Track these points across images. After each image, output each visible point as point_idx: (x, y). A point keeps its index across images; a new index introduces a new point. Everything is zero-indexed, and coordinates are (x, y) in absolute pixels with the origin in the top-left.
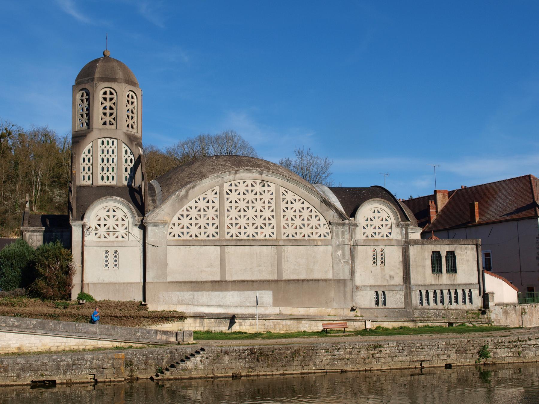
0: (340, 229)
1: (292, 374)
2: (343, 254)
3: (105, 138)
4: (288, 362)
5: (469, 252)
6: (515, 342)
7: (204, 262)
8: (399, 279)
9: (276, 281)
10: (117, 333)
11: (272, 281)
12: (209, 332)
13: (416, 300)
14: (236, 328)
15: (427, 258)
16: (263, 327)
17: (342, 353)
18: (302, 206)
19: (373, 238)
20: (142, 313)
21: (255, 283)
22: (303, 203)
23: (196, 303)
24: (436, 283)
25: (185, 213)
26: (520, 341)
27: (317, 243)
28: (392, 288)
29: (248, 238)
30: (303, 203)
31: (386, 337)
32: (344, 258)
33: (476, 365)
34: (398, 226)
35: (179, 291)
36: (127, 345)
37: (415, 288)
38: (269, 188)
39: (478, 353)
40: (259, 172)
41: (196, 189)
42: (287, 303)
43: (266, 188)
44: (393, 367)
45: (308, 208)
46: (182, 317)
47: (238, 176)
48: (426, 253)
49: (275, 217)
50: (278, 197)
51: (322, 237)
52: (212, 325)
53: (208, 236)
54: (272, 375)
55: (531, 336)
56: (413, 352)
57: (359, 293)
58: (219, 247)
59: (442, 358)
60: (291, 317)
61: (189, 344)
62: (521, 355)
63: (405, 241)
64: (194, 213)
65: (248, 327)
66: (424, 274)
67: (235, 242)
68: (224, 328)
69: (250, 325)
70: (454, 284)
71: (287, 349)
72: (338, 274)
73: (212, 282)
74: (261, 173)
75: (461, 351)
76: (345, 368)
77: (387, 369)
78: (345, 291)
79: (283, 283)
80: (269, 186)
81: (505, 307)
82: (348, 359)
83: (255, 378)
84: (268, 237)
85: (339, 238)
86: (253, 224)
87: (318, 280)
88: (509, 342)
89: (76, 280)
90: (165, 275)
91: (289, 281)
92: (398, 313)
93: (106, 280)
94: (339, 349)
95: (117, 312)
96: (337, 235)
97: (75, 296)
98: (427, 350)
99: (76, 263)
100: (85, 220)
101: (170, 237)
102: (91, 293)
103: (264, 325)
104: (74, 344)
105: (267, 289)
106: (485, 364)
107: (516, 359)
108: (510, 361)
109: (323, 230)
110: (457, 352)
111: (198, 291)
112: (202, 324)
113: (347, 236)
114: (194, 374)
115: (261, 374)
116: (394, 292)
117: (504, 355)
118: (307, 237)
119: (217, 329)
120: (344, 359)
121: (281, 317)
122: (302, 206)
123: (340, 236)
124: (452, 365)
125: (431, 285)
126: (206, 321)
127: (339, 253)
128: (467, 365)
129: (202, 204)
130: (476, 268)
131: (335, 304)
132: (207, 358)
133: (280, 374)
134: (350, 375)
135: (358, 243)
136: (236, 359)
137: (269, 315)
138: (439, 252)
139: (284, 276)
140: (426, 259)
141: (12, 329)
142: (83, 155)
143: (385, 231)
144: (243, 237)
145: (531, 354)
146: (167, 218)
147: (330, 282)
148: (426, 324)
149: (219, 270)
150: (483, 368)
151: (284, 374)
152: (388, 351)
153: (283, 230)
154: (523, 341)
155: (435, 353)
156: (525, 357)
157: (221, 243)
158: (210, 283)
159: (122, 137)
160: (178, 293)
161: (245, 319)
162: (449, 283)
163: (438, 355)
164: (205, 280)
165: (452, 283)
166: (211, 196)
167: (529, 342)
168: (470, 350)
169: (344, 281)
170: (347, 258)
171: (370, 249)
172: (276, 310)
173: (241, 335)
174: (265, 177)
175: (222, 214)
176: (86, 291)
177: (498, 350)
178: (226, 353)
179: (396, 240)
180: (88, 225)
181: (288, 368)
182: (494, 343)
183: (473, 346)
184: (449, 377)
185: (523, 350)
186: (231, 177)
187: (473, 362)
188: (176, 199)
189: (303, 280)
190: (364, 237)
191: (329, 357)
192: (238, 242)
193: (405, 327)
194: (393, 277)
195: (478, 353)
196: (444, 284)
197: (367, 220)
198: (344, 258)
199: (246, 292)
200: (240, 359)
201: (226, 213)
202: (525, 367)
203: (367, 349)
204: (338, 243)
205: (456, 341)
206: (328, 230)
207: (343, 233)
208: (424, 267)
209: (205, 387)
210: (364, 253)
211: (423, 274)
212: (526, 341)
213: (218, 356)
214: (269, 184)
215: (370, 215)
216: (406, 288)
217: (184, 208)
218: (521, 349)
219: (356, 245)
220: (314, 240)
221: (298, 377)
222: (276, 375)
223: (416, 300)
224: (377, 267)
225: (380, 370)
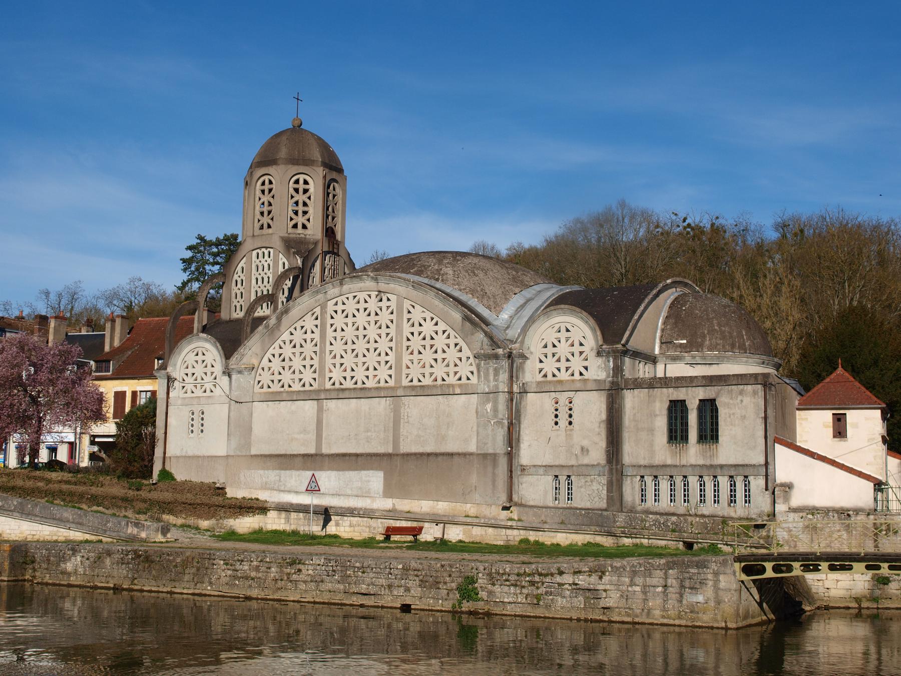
0: (492, 364)
1: (182, 594)
2: (495, 410)
3: (260, 248)
5: (747, 400)
6: (529, 575)
7: (284, 425)
8: (598, 454)
9: (389, 456)
10: (89, 521)
12: (295, 533)
13: (633, 496)
14: (331, 529)
15: (658, 413)
16: (367, 530)
17: (246, 567)
18: (436, 328)
19: (555, 379)
20: (218, 500)
21: (359, 458)
22: (436, 324)
23: (282, 488)
24: (674, 463)
26: (540, 575)
27: (454, 390)
28: (584, 470)
29: (411, 384)
30: (436, 324)
31: (308, 549)
32: (495, 416)
33: (454, 613)
34: (599, 354)
35: (263, 469)
37: (629, 471)
38: (388, 303)
39: (459, 589)
40: (372, 278)
43: (384, 304)
44: (317, 600)
45: (444, 332)
46: (260, 508)
47: (346, 287)
48: (658, 405)
49: (394, 349)
53: (304, 385)
54: (158, 592)
56: (349, 576)
58: (315, 402)
59: (395, 593)
60: (408, 515)
61: (155, 542)
62: (541, 603)
63: (613, 383)
64: (288, 351)
65: (347, 529)
66: (651, 445)
67: (336, 393)
68: (316, 529)
69: (350, 526)
70: (712, 466)
72: (486, 444)
73: (304, 456)
74: (376, 280)
75: (430, 583)
77: (308, 602)
78: (494, 474)
79: (399, 458)
80: (388, 300)
81: (810, 516)
82: (253, 579)
83: (139, 594)
84: (382, 384)
85: (489, 381)
87: (451, 455)
88: (518, 575)
90: (249, 445)
93: (190, 453)
94: (242, 561)
98: (371, 575)
100: (169, 369)
101: (257, 389)
102: (173, 471)
103: (370, 527)
104: (48, 533)
105: (376, 469)
106: (470, 613)
107: (529, 609)
108: (519, 611)
109: (465, 369)
111: (286, 469)
112: (288, 520)
113: (504, 376)
114: (73, 580)
115: (145, 588)
116: (588, 479)
117: (508, 598)
118: (439, 382)
119: (306, 529)
121: (412, 516)
122: (436, 328)
123: (491, 378)
124: (412, 607)
126: (293, 515)
127: (489, 407)
128: (438, 611)
129: (298, 337)
130: (762, 433)
131: (477, 497)
132: (88, 559)
133: (167, 592)
135: (528, 389)
136: (118, 563)
138: (685, 401)
139: (401, 447)
140: (656, 416)
142: (236, 277)
143: (577, 364)
144: (349, 384)
145: (560, 601)
146: (255, 362)
147: (471, 457)
148: (638, 541)
149: (315, 437)
152: (310, 572)
154: (546, 575)
156: (548, 607)
157: (316, 395)
158: (300, 459)
159: (278, 244)
160: (261, 472)
162: (701, 462)
163: (390, 586)
164: (295, 453)
165: (708, 463)
166: (309, 323)
167: (558, 579)
168: (445, 583)
169: (494, 456)
170: (500, 416)
172: (388, 504)
174: (382, 286)
175: (323, 351)
176: (167, 468)
177: (497, 589)
178: (109, 553)
179: (595, 380)
181: (177, 584)
183: (450, 576)
185: (546, 593)
186: (336, 291)
187: (448, 606)
188: (265, 331)
189: (429, 455)
190: (539, 378)
191: (229, 572)
192: (340, 393)
193: (598, 545)
194: (588, 451)
195: (459, 589)
196: (691, 465)
197: (545, 346)
198: (495, 416)
199: (347, 472)
200: (122, 564)
203: (281, 566)
204: (487, 390)
205: (421, 564)
207: (496, 372)
208: (651, 431)
210: (537, 406)
211: (646, 439)
212: (552, 575)
213: (100, 558)
214: (389, 296)
215: (551, 337)
216: (611, 470)
217: (276, 345)
218: (542, 590)
219: (524, 392)
220: (449, 386)
221: (187, 599)
222: (162, 592)
223: (633, 496)
224: (559, 432)
225: (298, 602)
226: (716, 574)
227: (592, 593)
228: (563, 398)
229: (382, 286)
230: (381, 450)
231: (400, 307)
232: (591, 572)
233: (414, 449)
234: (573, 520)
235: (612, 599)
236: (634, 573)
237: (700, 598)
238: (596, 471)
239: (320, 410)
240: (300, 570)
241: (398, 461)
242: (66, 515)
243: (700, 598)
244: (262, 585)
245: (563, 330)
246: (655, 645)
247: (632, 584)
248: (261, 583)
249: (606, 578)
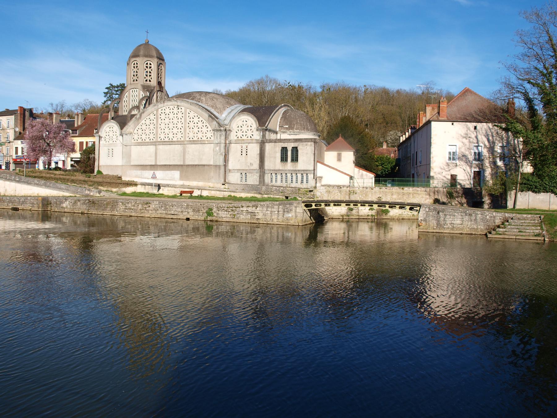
0: (219, 133)
2: (220, 149)
4: (105, 208)
5: (308, 147)
7: (145, 155)
8: (256, 165)
12: (148, 193)
14: (161, 191)
20: (119, 181)
28: (251, 171)
33: (205, 221)
36: (73, 195)
42: (187, 179)
43: (180, 110)
47: (165, 104)
50: (186, 115)
51: (209, 139)
55: (243, 205)
57: (231, 174)
68: (155, 191)
71: (104, 201)
76: (131, 214)
84: (179, 140)
89: (96, 164)
90: (130, 161)
95: (108, 180)
96: (217, 138)
97: (96, 170)
99: (97, 157)
100: (100, 133)
101: (133, 141)
109: (209, 134)
110: (194, 210)
112: (145, 188)
114: (66, 210)
117: (224, 216)
120: (130, 209)
127: (218, 148)
134: (133, 218)
137: (176, 185)
141: (37, 185)
142: (124, 99)
143: (249, 134)
145: (242, 217)
146: (132, 131)
153: (187, 135)
155: (180, 210)
156: (238, 218)
159: (140, 87)
161: (165, 187)
162: (292, 169)
163: (182, 212)
166: (152, 117)
167: (241, 209)
169: (219, 166)
171: (238, 146)
173: (162, 195)
174: (179, 104)
175: (157, 127)
177: (220, 212)
180: (101, 135)
184: (188, 225)
186: (162, 105)
187: (203, 218)
190: (236, 138)
201: (159, 126)
206: (212, 134)
208: (275, 158)
210: (235, 149)
215: (240, 124)
216: (260, 171)
217: (140, 125)
219: (230, 143)
226: (296, 207)
228: (244, 146)
230: (179, 164)
231: (186, 111)
233: (190, 164)
234: (247, 188)
235: (260, 216)
236: (268, 207)
237: (290, 215)
239: (156, 149)
241: (185, 167)
243: (290, 215)
244: (135, 211)
246: (274, 230)
247: (267, 210)
248: (135, 211)
249: (258, 209)
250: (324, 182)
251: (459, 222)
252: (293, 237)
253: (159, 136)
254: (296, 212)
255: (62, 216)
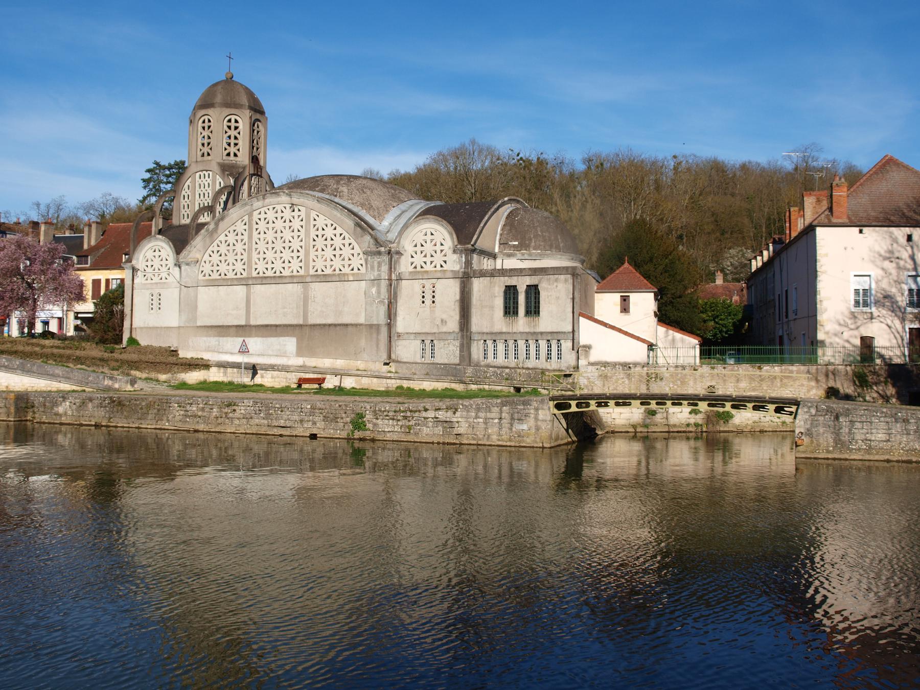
0: (377, 259)
2: (379, 292)
6: (403, 412)
7: (221, 305)
8: (453, 324)
9: (300, 326)
11: (297, 325)
13: (478, 354)
14: (258, 380)
20: (172, 359)
25: (215, 250)
26: (411, 411)
28: (443, 337)
33: (348, 439)
34: (454, 252)
35: (206, 336)
36: (79, 388)
37: (475, 337)
41: (226, 220)
43: (296, 213)
47: (267, 201)
48: (497, 289)
51: (356, 271)
52: (235, 375)
59: (305, 425)
63: (464, 273)
65: (270, 380)
66: (492, 318)
68: (247, 380)
73: (237, 326)
75: (330, 418)
76: (197, 427)
84: (295, 273)
86: (425, 256)
87: (347, 325)
90: (195, 319)
91: (314, 325)
92: (446, 371)
95: (151, 357)
96: (372, 268)
98: (288, 413)
100: (134, 262)
101: (201, 277)
106: (360, 439)
107: (403, 436)
109: (357, 262)
112: (225, 374)
113: (385, 268)
116: (446, 342)
119: (239, 380)
120: (195, 416)
122: (335, 232)
125: (501, 333)
126: (230, 370)
127: (374, 290)
131: (365, 356)
137: (288, 366)
141: (8, 369)
142: (183, 193)
144: (269, 273)
145: (425, 430)
146: (199, 256)
150: (357, 444)
151: (139, 428)
155: (296, 417)
156: (416, 434)
157: (246, 282)
159: (216, 168)
160: (205, 339)
161: (266, 370)
162: (527, 330)
163: (301, 421)
165: (532, 330)
166: (240, 227)
167: (424, 414)
169: (378, 327)
171: (417, 285)
172: (300, 361)
174: (295, 200)
175: (250, 249)
176: (134, 336)
177: (379, 422)
178: (91, 400)
180: (137, 267)
181: (143, 422)
182: (375, 411)
184: (314, 451)
186: (260, 203)
187: (344, 434)
189: (330, 325)
190: (411, 269)
191: (182, 413)
192: (263, 280)
193: (453, 390)
202: (416, 449)
206: (363, 262)
208: (492, 308)
209: (72, 434)
210: (409, 290)
212: (420, 411)
214: (300, 208)
215: (420, 239)
216: (462, 336)
217: (215, 244)
219: (400, 279)
223: (478, 354)
226: (537, 409)
227: (448, 424)
229: (295, 200)
230: (295, 322)
231: (308, 216)
232: (448, 409)
234: (435, 372)
235: (462, 429)
237: (525, 427)
238: (452, 336)
240: (234, 410)
241: (307, 330)
242: (57, 371)
244: (206, 420)
245: (429, 234)
247: (477, 417)
248: (206, 420)
249: (458, 414)
250: (594, 356)
251: (881, 436)
252: (532, 470)
253: (254, 266)
254: (536, 419)
255: (57, 433)
